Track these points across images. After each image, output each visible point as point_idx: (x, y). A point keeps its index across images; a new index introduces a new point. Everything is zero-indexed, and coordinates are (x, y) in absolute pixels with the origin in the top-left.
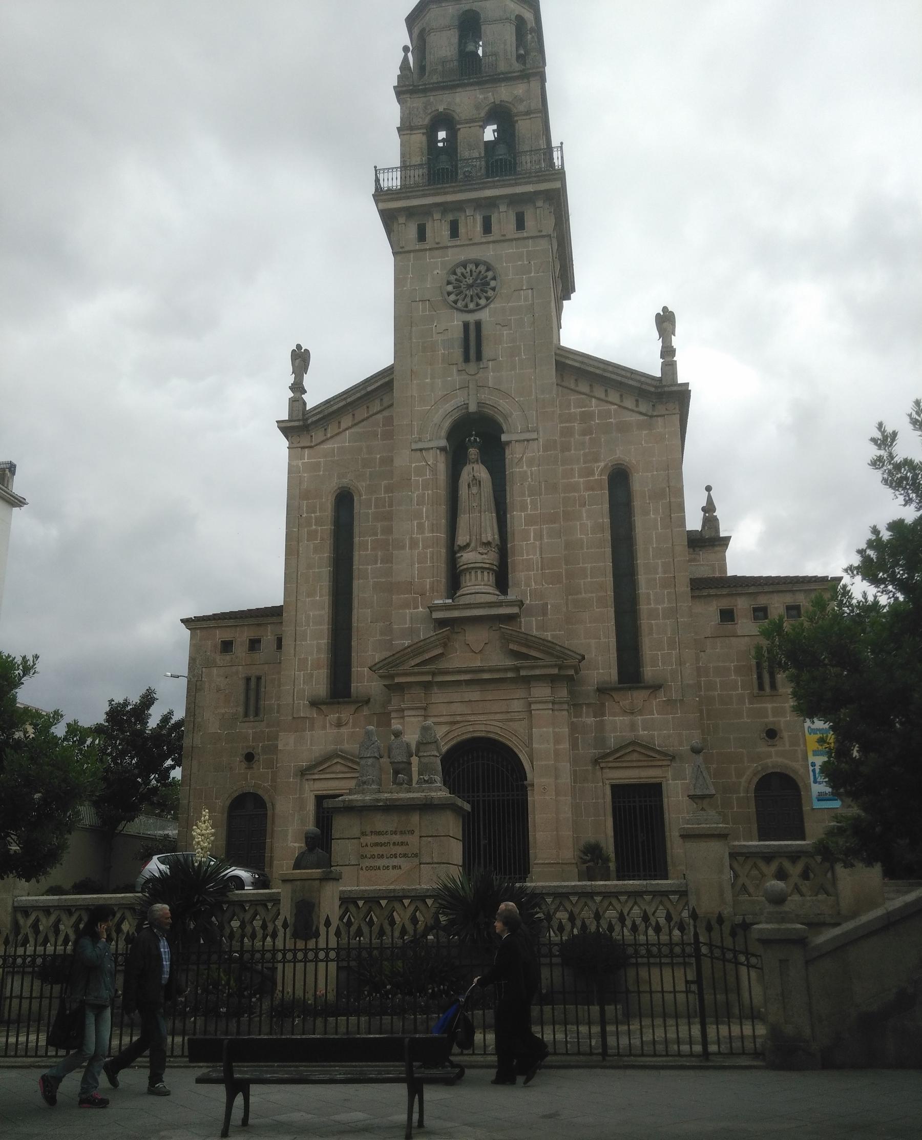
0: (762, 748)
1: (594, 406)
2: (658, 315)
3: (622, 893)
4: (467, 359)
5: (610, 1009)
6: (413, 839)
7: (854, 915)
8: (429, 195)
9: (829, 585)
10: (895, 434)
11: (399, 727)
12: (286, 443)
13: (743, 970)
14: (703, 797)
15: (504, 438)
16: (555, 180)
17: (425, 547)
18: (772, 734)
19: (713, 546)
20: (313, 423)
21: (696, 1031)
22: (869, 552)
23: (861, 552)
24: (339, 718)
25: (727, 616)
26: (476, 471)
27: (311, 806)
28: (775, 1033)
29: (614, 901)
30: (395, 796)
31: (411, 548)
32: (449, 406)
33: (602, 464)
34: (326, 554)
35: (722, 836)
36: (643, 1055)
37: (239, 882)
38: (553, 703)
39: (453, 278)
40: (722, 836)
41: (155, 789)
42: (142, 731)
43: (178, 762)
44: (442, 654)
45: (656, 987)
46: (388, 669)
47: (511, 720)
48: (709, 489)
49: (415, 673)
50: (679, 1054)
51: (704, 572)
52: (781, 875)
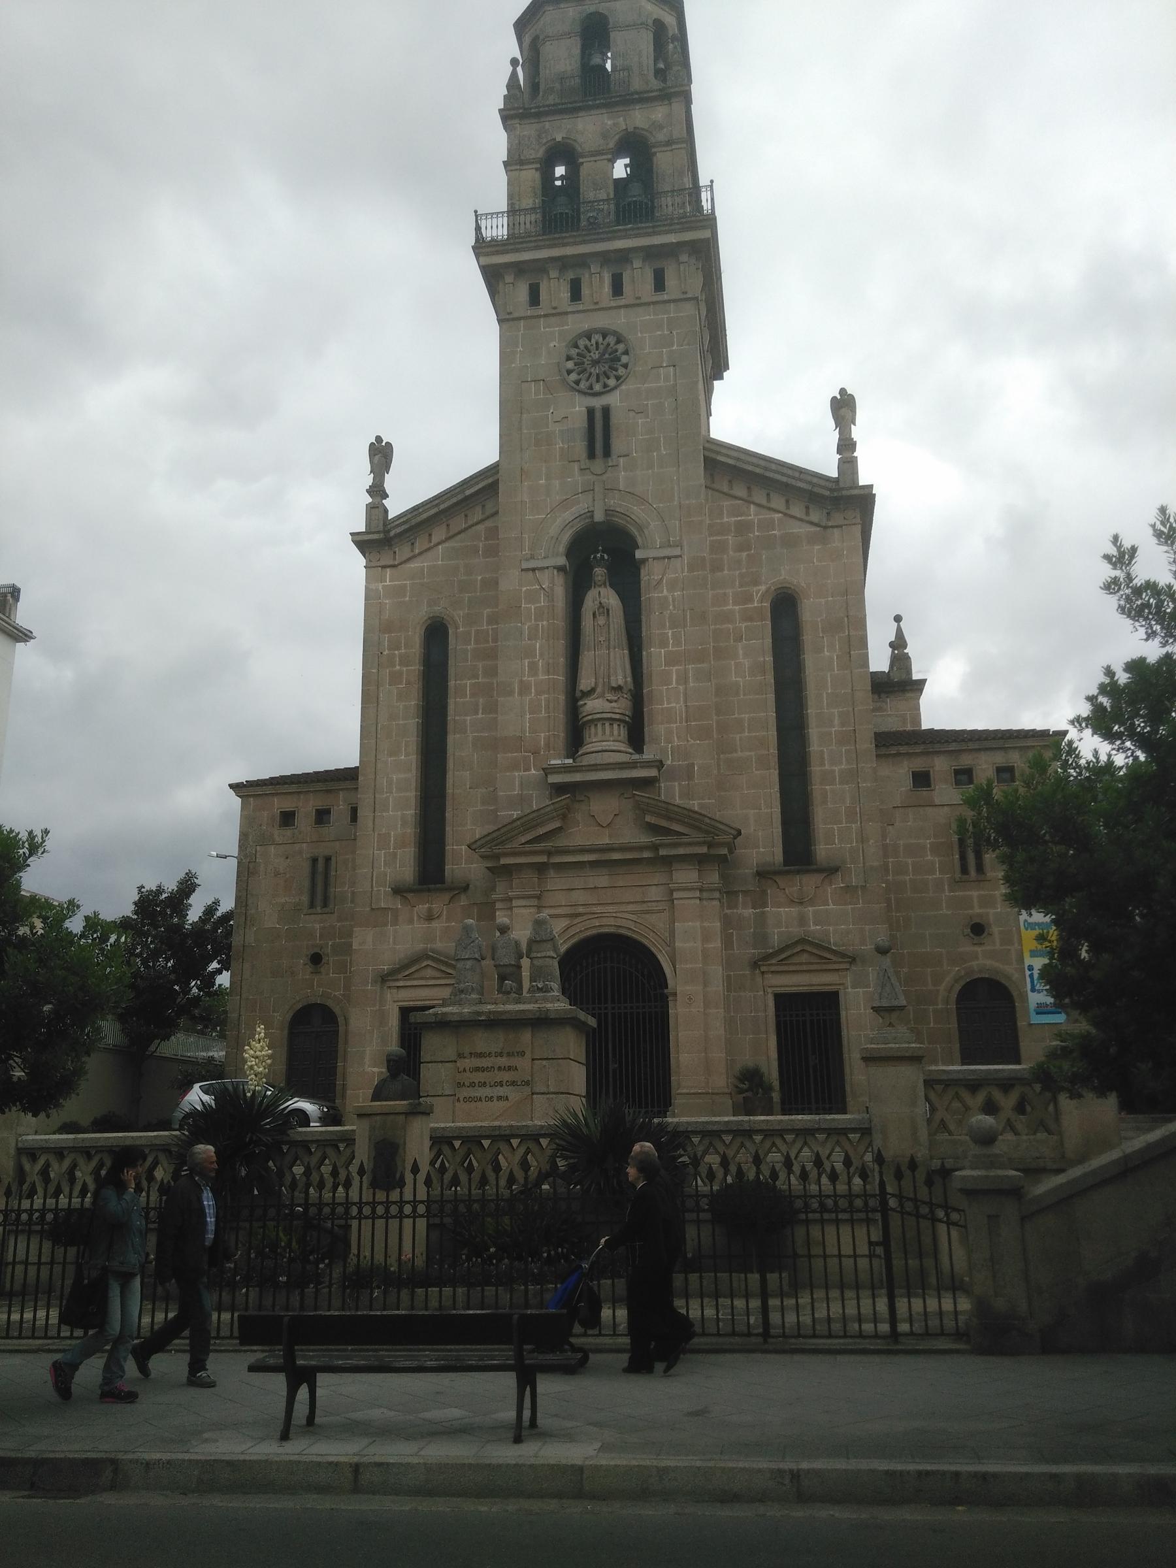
0: (967, 948)
1: (753, 514)
2: (834, 398)
4: (591, 455)
5: (772, 1278)
6: (524, 1063)
7: (1082, 1159)
9: (1051, 741)
10: (1133, 550)
11: (506, 920)
12: (362, 561)
13: (942, 1229)
14: (891, 1009)
15: (639, 554)
16: (704, 228)
17: (538, 693)
18: (978, 929)
19: (904, 691)
21: (882, 1305)
23: (1091, 699)
24: (430, 909)
25: (922, 779)
27: (394, 1021)
28: (982, 1308)
29: (779, 1142)
30: (501, 1008)
31: (520, 694)
32: (568, 515)
33: (763, 588)
34: (413, 701)
35: (915, 1059)
36: (814, 1336)
38: (701, 891)
39: (574, 352)
40: (915, 1059)
41: (197, 999)
42: (180, 927)
43: (226, 966)
44: (560, 828)
45: (832, 1250)
46: (491, 847)
48: (898, 619)
49: (525, 853)
50: (861, 1335)
51: (891, 724)
52: (990, 1108)
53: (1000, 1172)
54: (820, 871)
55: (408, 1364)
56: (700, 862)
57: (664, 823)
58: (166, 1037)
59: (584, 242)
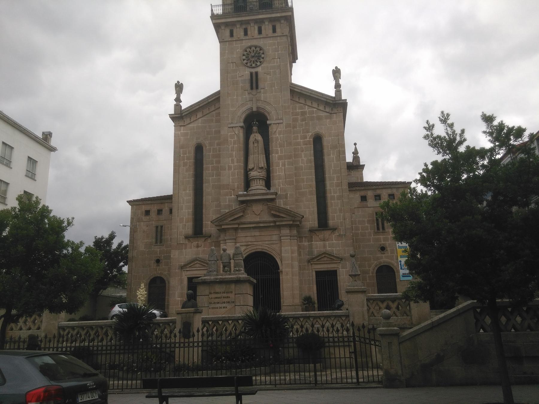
0: (379, 255)
1: (307, 109)
2: (333, 70)
3: (321, 316)
4: (252, 88)
5: (318, 365)
6: (232, 296)
7: (419, 323)
8: (235, 17)
9: (407, 185)
10: (433, 126)
11: (225, 247)
12: (173, 124)
13: (373, 347)
14: (355, 275)
15: (268, 122)
16: (290, 11)
18: (383, 249)
19: (357, 169)
20: (184, 115)
21: (354, 373)
22: (423, 173)
23: (420, 174)
25: (364, 198)
26: (256, 137)
27: (186, 282)
28: (386, 373)
29: (318, 320)
30: (224, 277)
31: (228, 170)
32: (244, 109)
33: (310, 134)
34: (192, 172)
35: (363, 292)
36: (332, 383)
37: (154, 315)
38: (291, 236)
39: (245, 53)
40: (363, 292)
41: (116, 275)
42: (110, 250)
43: (126, 264)
44: (242, 216)
45: (337, 356)
46: (219, 222)
47: (274, 244)
48: (355, 144)
49: (230, 224)
50: (347, 383)
51: (354, 180)
52: (388, 307)
53: (392, 328)
54: (330, 229)
55: (199, 394)
56: (290, 227)
57: (278, 214)
58: (105, 289)
59: (249, 16)
